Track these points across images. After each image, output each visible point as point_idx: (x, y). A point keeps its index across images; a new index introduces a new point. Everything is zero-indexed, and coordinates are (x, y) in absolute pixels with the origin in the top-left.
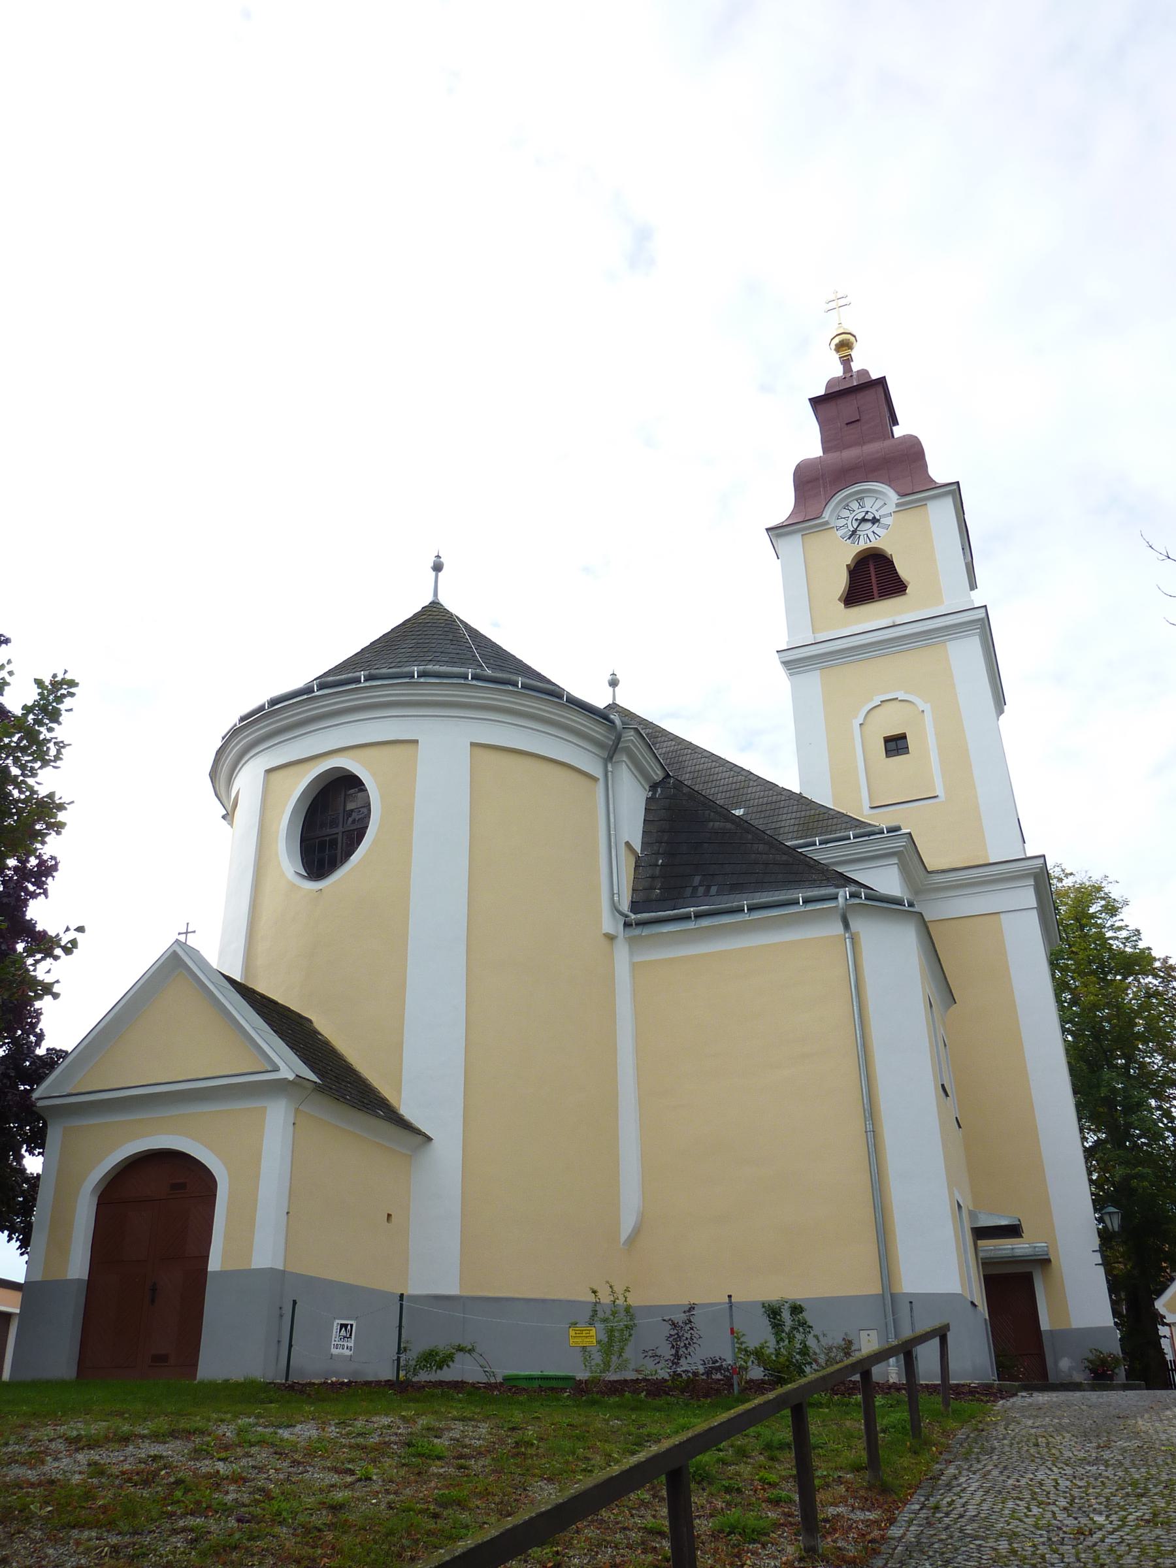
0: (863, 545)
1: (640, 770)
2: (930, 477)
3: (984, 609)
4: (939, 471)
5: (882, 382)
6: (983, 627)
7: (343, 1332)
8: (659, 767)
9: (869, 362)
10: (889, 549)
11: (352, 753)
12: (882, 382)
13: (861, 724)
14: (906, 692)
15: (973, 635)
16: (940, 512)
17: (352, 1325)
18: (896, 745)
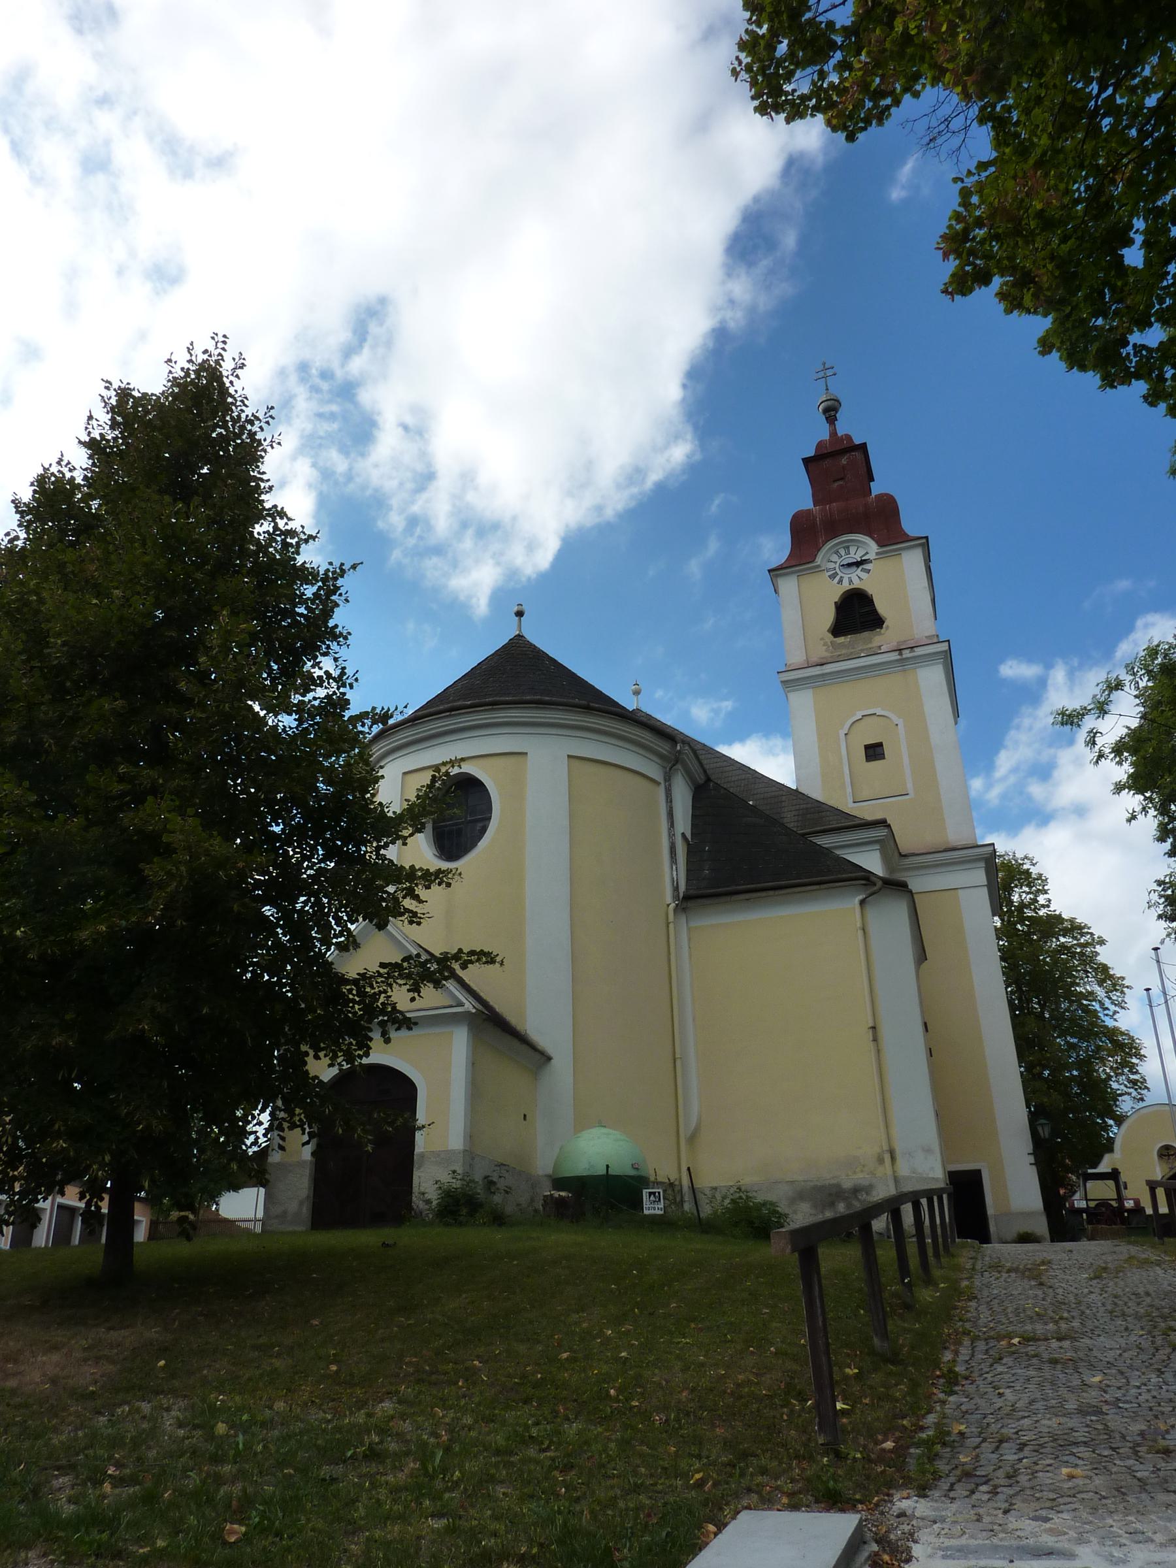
0: (846, 586)
1: (689, 774)
2: (904, 531)
3: (947, 644)
4: (910, 524)
5: (863, 447)
6: (945, 658)
7: (652, 1198)
8: (702, 771)
9: (850, 426)
10: (870, 590)
11: (475, 761)
12: (863, 447)
13: (846, 734)
14: (883, 709)
15: (938, 663)
16: (912, 560)
17: (659, 1193)
18: (874, 752)
